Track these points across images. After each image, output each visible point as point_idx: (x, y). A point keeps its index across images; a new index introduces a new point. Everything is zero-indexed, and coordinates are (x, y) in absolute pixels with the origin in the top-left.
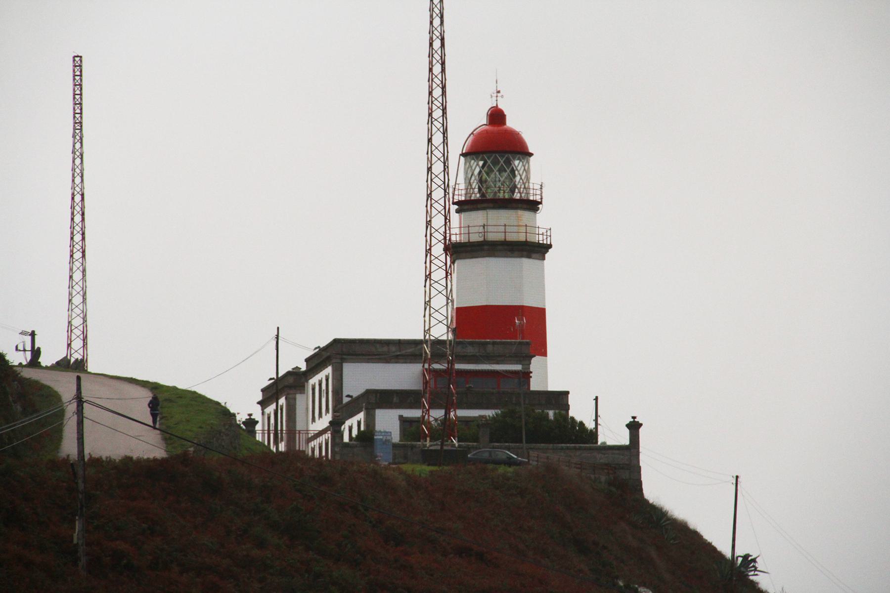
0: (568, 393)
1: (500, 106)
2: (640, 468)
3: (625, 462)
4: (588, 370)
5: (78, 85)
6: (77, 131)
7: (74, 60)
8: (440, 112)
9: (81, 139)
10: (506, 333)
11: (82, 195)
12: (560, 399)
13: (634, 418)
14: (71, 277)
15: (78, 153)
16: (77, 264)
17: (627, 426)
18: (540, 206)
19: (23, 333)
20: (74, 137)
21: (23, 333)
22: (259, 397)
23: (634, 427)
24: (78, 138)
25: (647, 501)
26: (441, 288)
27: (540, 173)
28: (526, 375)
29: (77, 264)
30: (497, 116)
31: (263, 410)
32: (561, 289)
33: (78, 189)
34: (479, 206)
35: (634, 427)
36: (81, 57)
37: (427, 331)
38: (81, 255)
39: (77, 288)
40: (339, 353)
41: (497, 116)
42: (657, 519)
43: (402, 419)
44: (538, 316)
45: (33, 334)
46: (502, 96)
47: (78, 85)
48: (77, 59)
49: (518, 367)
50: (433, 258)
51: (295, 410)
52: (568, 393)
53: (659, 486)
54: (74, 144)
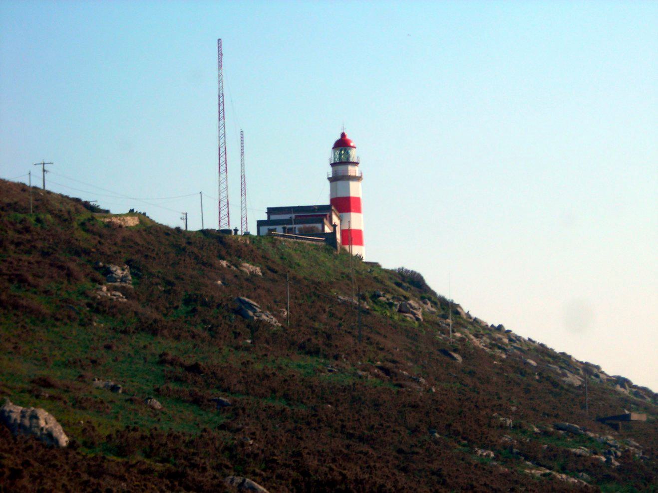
27: (354, 154)
30: (343, 135)
36: (399, 491)
41: (343, 135)
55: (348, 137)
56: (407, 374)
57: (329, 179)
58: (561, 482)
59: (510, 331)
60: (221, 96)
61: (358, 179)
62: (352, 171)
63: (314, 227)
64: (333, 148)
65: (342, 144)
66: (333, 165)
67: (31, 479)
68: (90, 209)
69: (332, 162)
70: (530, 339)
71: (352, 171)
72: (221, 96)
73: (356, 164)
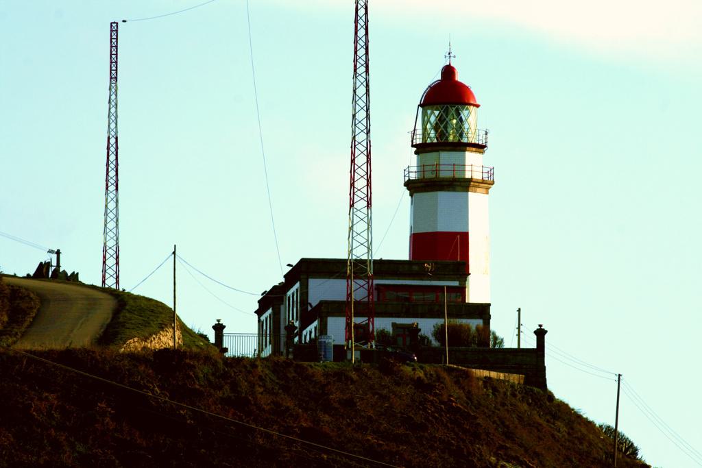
0: (489, 305)
1: (452, 65)
2: (545, 367)
3: (531, 363)
4: (507, 287)
5: (114, 47)
6: (113, 85)
7: (111, 26)
8: (363, 69)
9: (116, 91)
10: (442, 252)
11: (117, 139)
12: (483, 311)
13: (540, 326)
14: (106, 206)
15: (113, 103)
16: (112, 195)
17: (535, 332)
18: (485, 149)
19: (50, 251)
20: (110, 89)
21: (50, 251)
22: (257, 307)
23: (540, 334)
24: (113, 90)
25: (550, 397)
26: (362, 216)
27: (475, 122)
28: (462, 290)
29: (112, 195)
30: (448, 72)
31: (259, 318)
32: (482, 219)
33: (113, 133)
34: (427, 149)
35: (540, 334)
36: (111, 23)
37: (351, 252)
38: (365, 183)
39: (111, 215)
40: (305, 270)
41: (448, 72)
42: (563, 413)
43: (394, 325)
44: (465, 236)
45: (58, 253)
46: (454, 57)
47: (114, 47)
48: (114, 25)
49: (456, 283)
50: (356, 190)
51: (390, 317)
52: (489, 305)
53: (566, 382)
54: (110, 96)
55: (460, 77)
56: (388, 349)
57: (409, 184)
58: (464, 367)
59: (41, 263)
60: (113, 146)
61: (486, 184)
62: (473, 164)
63: (461, 326)
64: (420, 105)
65: (447, 95)
66: (421, 149)
67: (229, 375)
68: (106, 332)
69: (418, 141)
70: (262, 294)
71: (473, 164)
72: (113, 146)
73: (480, 147)
